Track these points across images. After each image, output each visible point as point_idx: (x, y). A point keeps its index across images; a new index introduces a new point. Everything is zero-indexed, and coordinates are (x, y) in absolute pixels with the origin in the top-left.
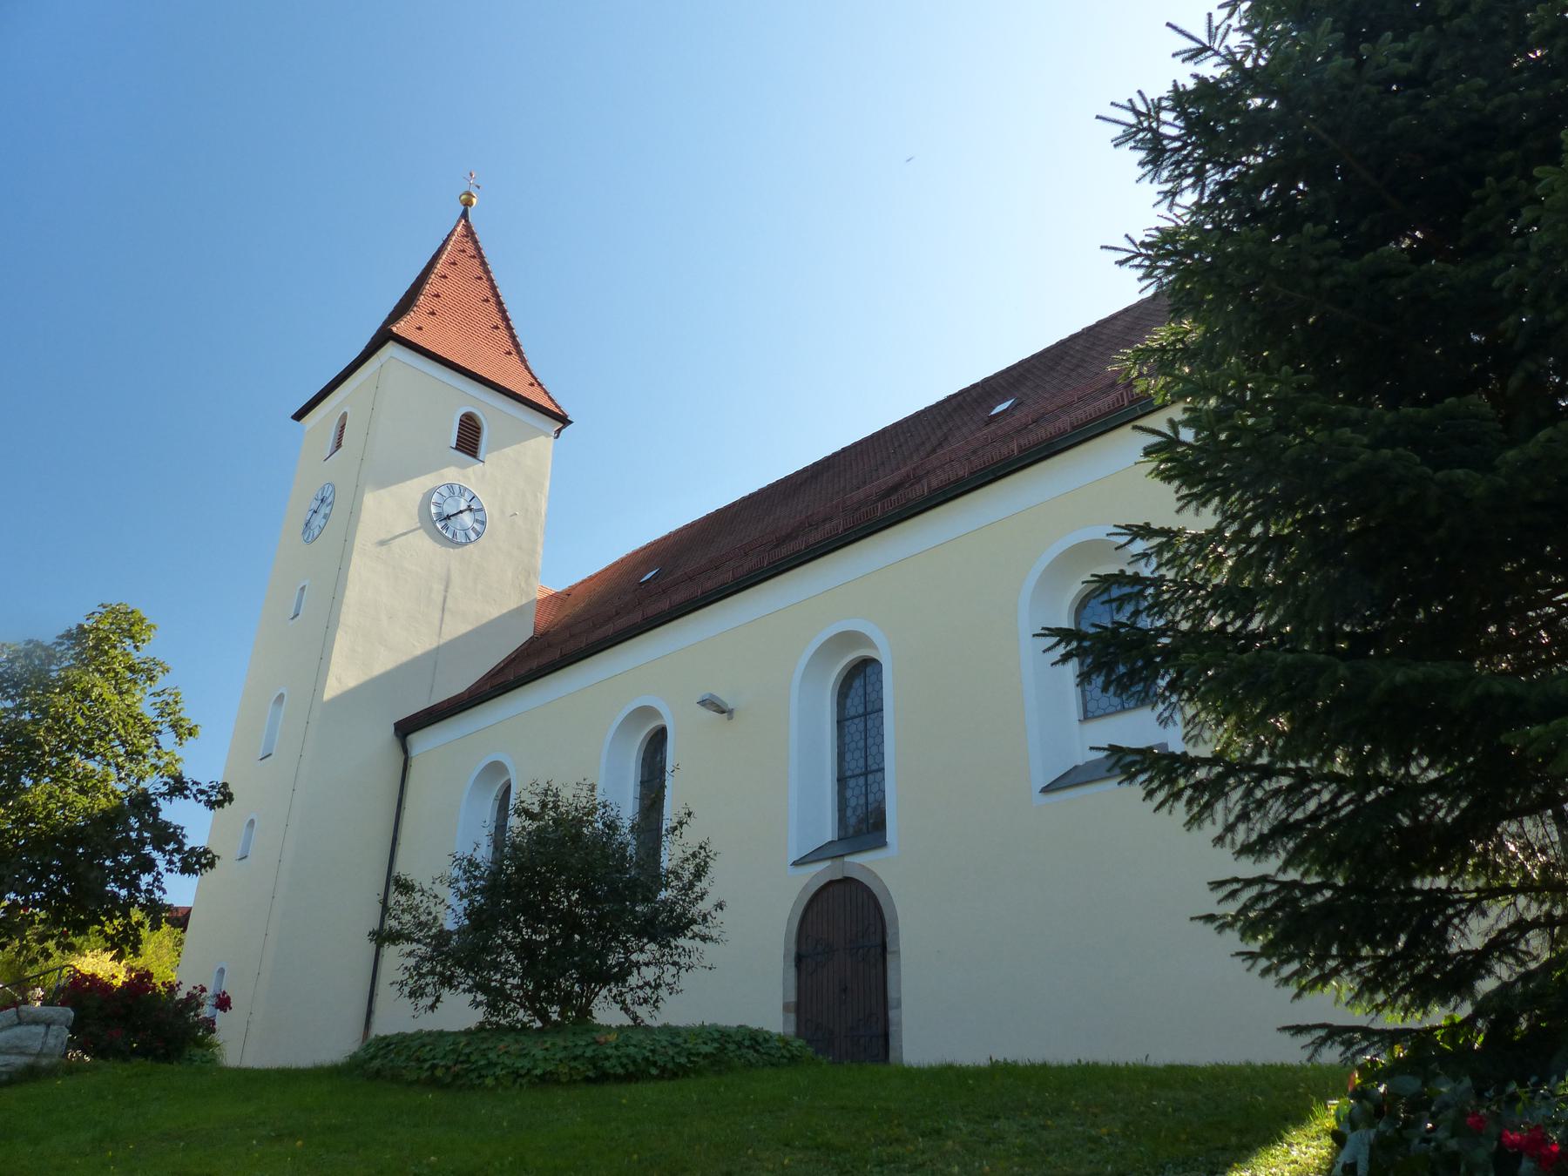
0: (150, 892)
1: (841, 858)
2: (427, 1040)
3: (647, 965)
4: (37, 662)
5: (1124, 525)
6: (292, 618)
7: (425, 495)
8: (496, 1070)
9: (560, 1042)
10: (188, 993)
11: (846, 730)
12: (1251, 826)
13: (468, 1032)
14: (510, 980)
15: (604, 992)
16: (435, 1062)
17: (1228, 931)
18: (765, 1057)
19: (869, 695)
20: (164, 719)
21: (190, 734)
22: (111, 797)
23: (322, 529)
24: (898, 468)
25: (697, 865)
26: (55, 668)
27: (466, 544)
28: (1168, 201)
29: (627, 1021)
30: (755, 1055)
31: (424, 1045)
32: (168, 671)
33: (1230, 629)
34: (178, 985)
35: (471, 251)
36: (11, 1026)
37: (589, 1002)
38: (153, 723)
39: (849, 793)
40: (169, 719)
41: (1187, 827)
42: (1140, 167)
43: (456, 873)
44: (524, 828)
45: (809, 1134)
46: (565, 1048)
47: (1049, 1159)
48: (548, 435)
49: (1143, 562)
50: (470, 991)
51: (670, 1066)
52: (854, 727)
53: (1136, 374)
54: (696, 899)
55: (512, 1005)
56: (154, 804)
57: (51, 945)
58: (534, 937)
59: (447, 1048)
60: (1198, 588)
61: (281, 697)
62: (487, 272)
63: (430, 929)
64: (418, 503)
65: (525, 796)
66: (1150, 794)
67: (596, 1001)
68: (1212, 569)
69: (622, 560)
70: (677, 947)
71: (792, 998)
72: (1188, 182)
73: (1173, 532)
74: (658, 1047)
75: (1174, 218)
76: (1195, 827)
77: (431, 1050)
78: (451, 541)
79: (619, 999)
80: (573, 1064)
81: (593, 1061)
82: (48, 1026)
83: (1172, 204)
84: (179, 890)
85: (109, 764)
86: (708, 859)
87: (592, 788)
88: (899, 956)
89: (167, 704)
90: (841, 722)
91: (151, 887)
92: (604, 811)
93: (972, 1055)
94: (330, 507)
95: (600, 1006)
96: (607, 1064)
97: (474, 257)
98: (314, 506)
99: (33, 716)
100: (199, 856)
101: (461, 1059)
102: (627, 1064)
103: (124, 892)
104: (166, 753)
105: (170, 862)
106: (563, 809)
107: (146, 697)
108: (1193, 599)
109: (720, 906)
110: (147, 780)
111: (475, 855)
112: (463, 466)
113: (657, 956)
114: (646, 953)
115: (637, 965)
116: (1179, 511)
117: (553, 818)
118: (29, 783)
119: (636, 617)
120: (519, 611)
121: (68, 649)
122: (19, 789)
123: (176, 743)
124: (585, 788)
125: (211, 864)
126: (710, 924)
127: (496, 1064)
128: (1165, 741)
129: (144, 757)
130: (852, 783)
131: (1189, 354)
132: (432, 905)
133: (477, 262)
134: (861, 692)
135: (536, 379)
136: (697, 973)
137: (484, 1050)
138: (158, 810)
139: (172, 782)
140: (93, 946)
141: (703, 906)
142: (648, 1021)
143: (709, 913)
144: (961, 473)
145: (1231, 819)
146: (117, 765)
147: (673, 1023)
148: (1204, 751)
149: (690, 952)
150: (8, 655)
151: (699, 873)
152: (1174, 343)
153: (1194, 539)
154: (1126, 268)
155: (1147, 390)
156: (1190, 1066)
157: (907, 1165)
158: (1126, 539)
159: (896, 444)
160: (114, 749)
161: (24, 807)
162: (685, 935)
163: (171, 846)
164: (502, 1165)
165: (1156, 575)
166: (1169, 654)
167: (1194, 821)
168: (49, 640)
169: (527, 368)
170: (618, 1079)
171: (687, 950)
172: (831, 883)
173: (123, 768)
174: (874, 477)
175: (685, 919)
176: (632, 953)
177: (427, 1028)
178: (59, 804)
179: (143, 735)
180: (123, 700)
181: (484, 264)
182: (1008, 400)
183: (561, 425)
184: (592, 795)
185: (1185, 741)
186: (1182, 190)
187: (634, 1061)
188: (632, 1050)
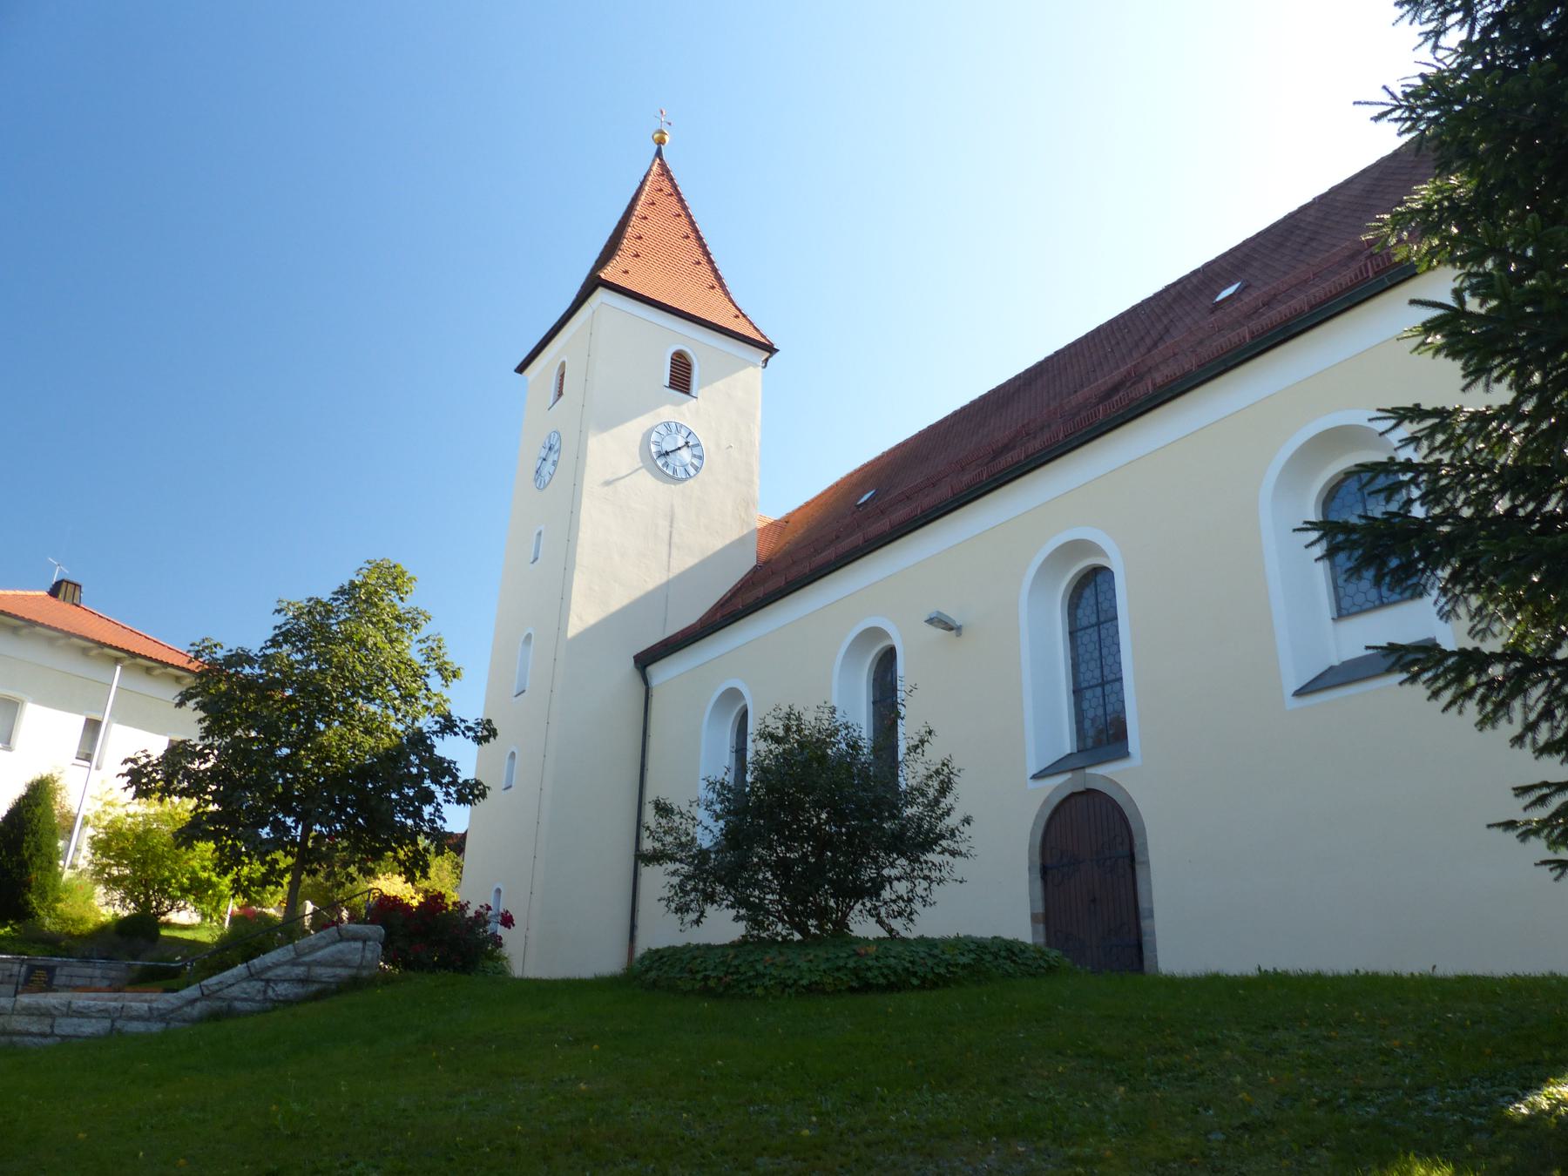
0: (432, 821)
1: (1082, 771)
2: (697, 953)
3: (898, 879)
4: (318, 618)
5: (1389, 408)
6: (533, 563)
7: (644, 435)
8: (764, 980)
9: (822, 953)
10: (476, 912)
11: (1079, 640)
12: (1555, 724)
13: (733, 945)
14: (769, 897)
15: (858, 906)
16: (707, 973)
17: (1532, 838)
18: (1022, 967)
19: (1101, 603)
20: (431, 663)
21: (454, 676)
22: (393, 737)
23: (552, 476)
24: (1118, 367)
25: (942, 782)
26: (334, 621)
27: (686, 480)
28: (1430, 43)
29: (883, 934)
30: (1012, 965)
31: (695, 958)
32: (430, 619)
33: (1521, 512)
34: (466, 905)
35: (668, 189)
36: (333, 943)
37: (845, 915)
38: (421, 667)
39: (1086, 705)
40: (434, 664)
41: (1479, 727)
42: (1397, 8)
43: (712, 796)
44: (771, 751)
45: (1080, 1043)
46: (828, 959)
47: (1339, 1070)
48: (755, 365)
49: (1412, 447)
50: (732, 906)
51: (930, 976)
52: (1087, 638)
53: (1394, 241)
54: (942, 815)
55: (771, 918)
56: (429, 742)
57: (352, 869)
58: (788, 855)
59: (717, 961)
60: (1478, 470)
61: (529, 637)
62: (685, 208)
63: (690, 850)
64: (638, 444)
65: (770, 721)
66: (1435, 694)
67: (851, 915)
68: (1496, 448)
69: (837, 484)
70: (926, 862)
71: (1040, 909)
72: (1454, 18)
73: (1448, 412)
74: (917, 959)
75: (1435, 62)
76: (1488, 727)
77: (702, 962)
78: (672, 477)
79: (874, 913)
80: (836, 974)
81: (855, 972)
82: (365, 942)
83: (1436, 47)
84: (456, 818)
85: (387, 707)
86: (951, 776)
87: (833, 711)
88: (1149, 867)
89: (432, 649)
90: (1073, 634)
91: (432, 817)
92: (846, 732)
93: (1239, 962)
94: (557, 455)
95: (856, 919)
96: (869, 974)
97: (671, 195)
98: (543, 454)
99: (319, 667)
100: (472, 788)
101: (731, 970)
102: (888, 974)
103: (410, 822)
104: (435, 695)
105: (447, 794)
106: (807, 732)
107: (413, 644)
108: (1476, 485)
109: (967, 821)
110: (420, 720)
111: (727, 778)
112: (678, 404)
113: (908, 870)
114: (897, 868)
115: (890, 880)
116: (1464, 389)
117: (797, 741)
118: (322, 727)
119: (857, 539)
120: (741, 541)
121: (343, 604)
122: (315, 733)
123: (443, 685)
124: (826, 710)
125: (483, 795)
126: (958, 839)
127: (764, 976)
128: (1432, 637)
129: (416, 699)
130: (1088, 694)
131: (1455, 211)
132: (690, 827)
133: (674, 199)
134: (1092, 601)
135: (740, 311)
136: (950, 886)
137: (751, 962)
138: (433, 746)
139: (442, 721)
140: (384, 869)
141: (952, 821)
142: (904, 934)
143: (957, 828)
144: (1187, 367)
145: (1532, 717)
146: (394, 708)
147: (929, 935)
148: (1492, 646)
149: (940, 866)
150: (294, 612)
151: (945, 789)
152: (1439, 202)
153: (1474, 416)
154: (1384, 121)
155: (1408, 258)
156: (1484, 977)
157: (1185, 1075)
158: (1392, 422)
159: (1113, 342)
160: (390, 693)
161: (321, 748)
162: (934, 850)
163: (447, 779)
164: (784, 1069)
165: (1431, 460)
166: (1450, 542)
167: (1486, 721)
168: (326, 596)
169: (731, 301)
170: (883, 989)
171: (938, 865)
172: (1072, 795)
173: (399, 710)
174: (1092, 380)
175: (933, 834)
176: (883, 868)
177: (694, 942)
178: (350, 745)
179: (413, 679)
180: (393, 648)
181: (681, 200)
182: (1233, 284)
183: (768, 354)
184: (834, 718)
185: (1472, 635)
186: (1447, 29)
187: (895, 972)
188: (892, 961)
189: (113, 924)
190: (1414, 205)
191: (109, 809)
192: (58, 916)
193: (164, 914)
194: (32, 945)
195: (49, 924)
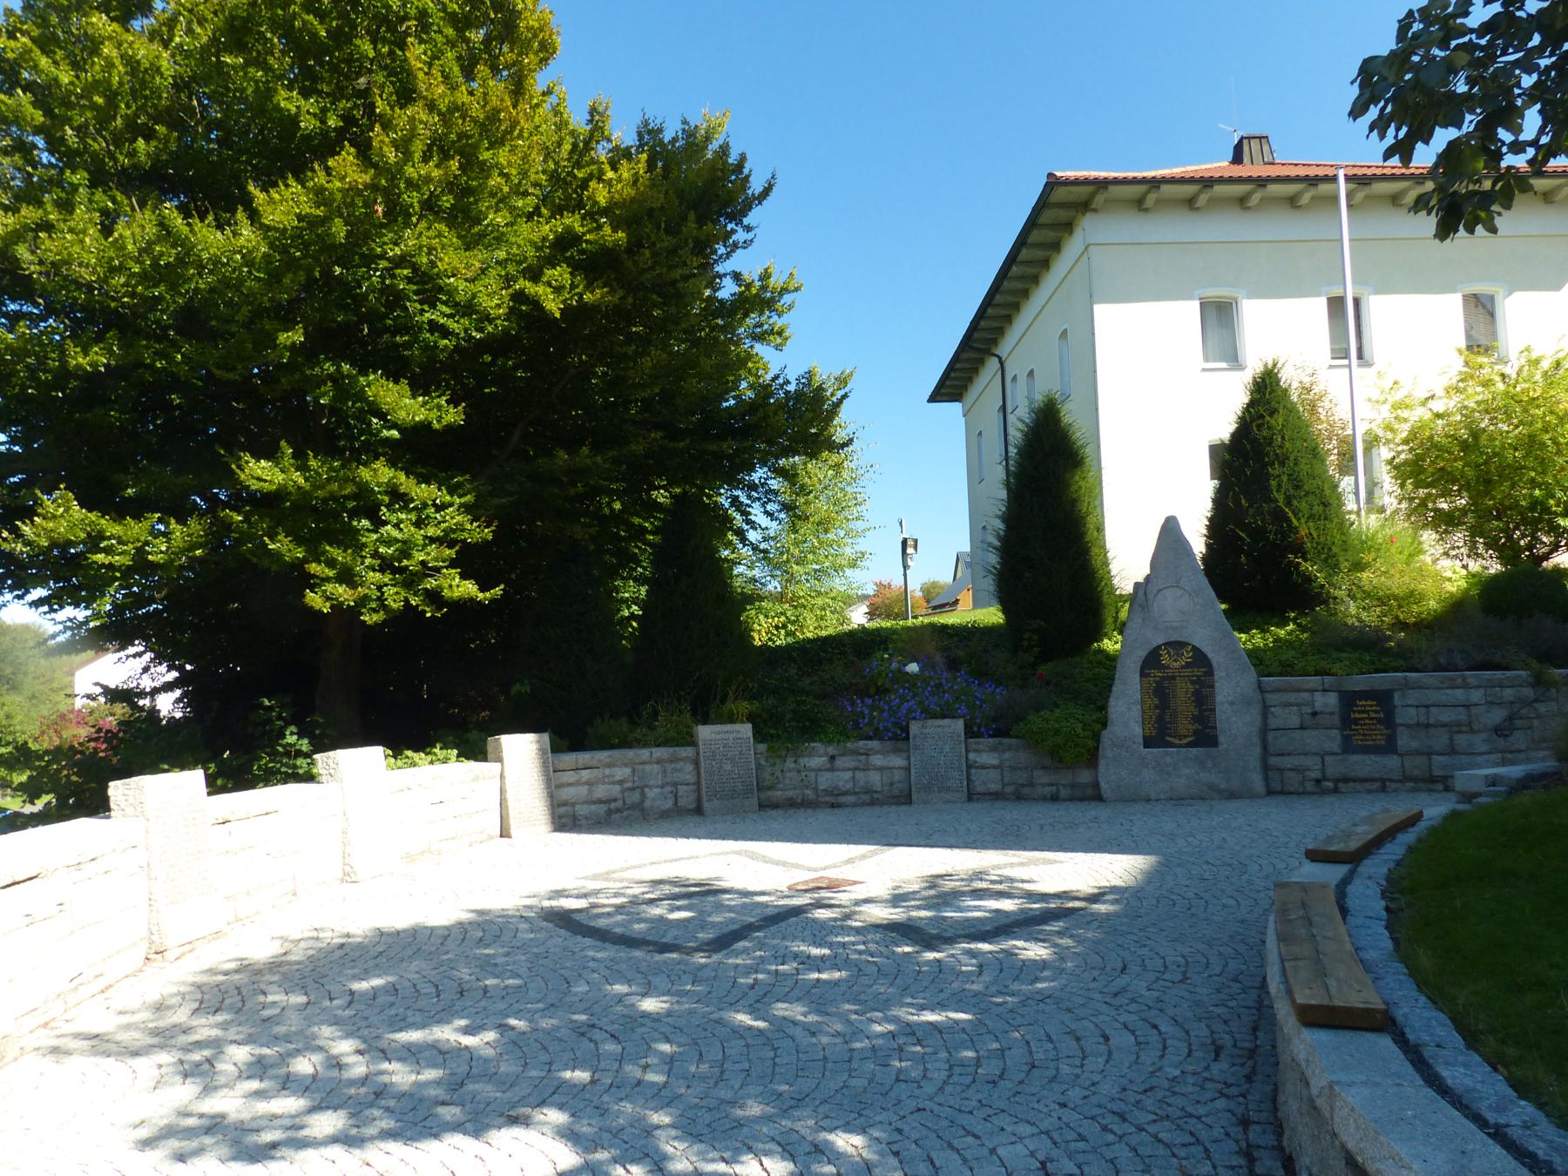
189: (1474, 592)
191: (1404, 414)
192: (1367, 595)
193: (1546, 557)
194: (1335, 655)
195: (1352, 611)
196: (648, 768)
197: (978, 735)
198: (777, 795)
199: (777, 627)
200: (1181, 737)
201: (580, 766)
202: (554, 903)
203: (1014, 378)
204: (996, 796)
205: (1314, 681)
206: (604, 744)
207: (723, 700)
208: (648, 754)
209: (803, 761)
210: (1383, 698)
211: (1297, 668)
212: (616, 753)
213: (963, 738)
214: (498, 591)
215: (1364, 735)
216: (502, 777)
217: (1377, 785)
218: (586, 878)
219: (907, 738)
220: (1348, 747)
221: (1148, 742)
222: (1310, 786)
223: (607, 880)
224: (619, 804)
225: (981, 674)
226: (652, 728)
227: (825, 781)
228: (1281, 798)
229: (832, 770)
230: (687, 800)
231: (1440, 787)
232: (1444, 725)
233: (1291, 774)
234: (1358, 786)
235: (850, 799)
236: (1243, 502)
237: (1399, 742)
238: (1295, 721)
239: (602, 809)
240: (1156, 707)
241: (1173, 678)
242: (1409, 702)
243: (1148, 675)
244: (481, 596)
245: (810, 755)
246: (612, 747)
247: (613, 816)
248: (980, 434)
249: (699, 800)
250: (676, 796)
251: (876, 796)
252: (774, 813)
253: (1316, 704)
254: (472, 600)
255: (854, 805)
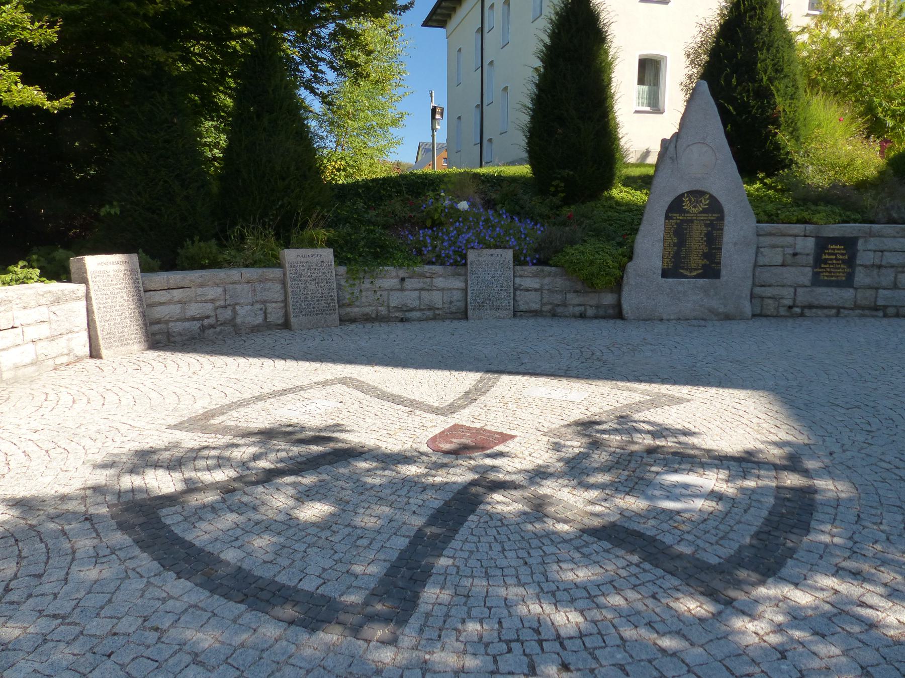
190: (145, 72)
196: (238, 287)
197: (525, 263)
198: (355, 311)
199: (339, 170)
200: (691, 270)
201: (172, 286)
202: (136, 481)
203: (492, 6)
204: (536, 314)
205: (798, 228)
206: (195, 264)
207: (303, 227)
208: (238, 275)
209: (379, 283)
210: (850, 243)
211: (781, 217)
212: (207, 273)
213: (511, 266)
214: (68, 101)
215: (830, 272)
216: (88, 298)
217: (834, 311)
218: (178, 427)
219: (465, 264)
220: (817, 281)
221: (665, 274)
222: (783, 311)
223: (205, 429)
224: (212, 321)
225: (519, 211)
226: (240, 250)
227: (396, 299)
228: (773, 320)
229: (402, 290)
230: (275, 316)
231: (881, 314)
232: (892, 266)
233: (770, 301)
234: (819, 312)
235: (417, 314)
236: (734, 80)
237: (856, 279)
238: (779, 260)
239: (196, 325)
240: (675, 245)
241: (692, 221)
242: (870, 247)
243: (671, 218)
244: (47, 104)
245: (384, 277)
246: (203, 267)
247: (207, 332)
248: (460, 50)
249: (286, 315)
250: (265, 313)
251: (437, 312)
252: (353, 326)
253: (797, 247)
254: (37, 109)
255: (420, 320)
